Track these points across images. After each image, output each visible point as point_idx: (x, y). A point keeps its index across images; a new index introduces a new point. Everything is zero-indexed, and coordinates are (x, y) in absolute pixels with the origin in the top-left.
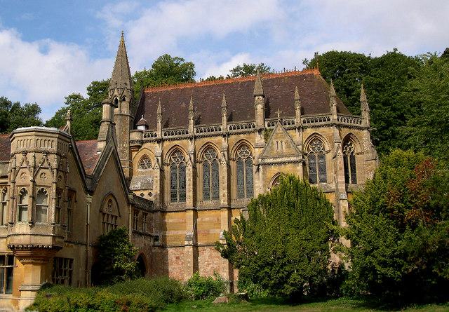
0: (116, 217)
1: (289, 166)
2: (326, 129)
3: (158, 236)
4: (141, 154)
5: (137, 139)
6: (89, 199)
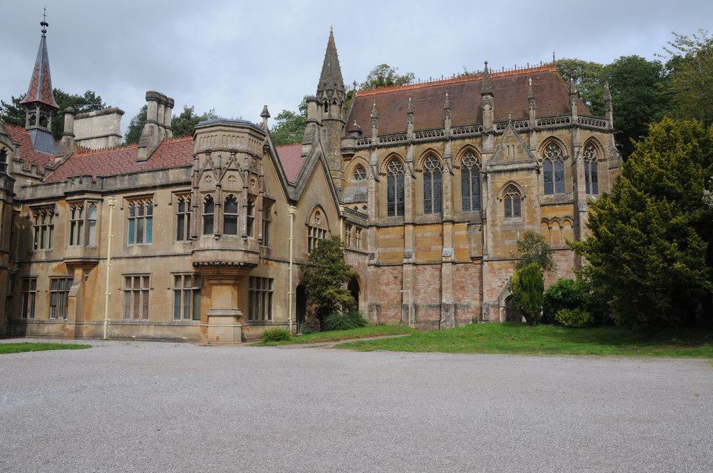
0: (325, 231)
1: (520, 173)
2: (565, 132)
3: (373, 254)
4: (354, 163)
5: (350, 146)
6: (291, 209)
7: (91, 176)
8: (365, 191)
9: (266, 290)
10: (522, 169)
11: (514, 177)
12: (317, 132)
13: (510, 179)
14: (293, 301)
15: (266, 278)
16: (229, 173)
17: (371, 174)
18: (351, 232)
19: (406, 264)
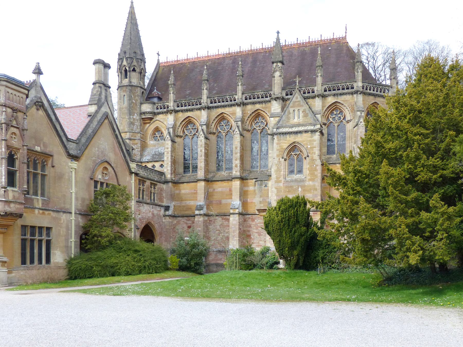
1: (304, 135)
2: (348, 97)
3: (169, 207)
4: (152, 127)
5: (148, 110)
6: (74, 164)
9: (43, 238)
10: (306, 132)
11: (299, 138)
13: (295, 141)
14: (75, 248)
15: (44, 227)
17: (168, 136)
18: (145, 187)
19: (197, 215)
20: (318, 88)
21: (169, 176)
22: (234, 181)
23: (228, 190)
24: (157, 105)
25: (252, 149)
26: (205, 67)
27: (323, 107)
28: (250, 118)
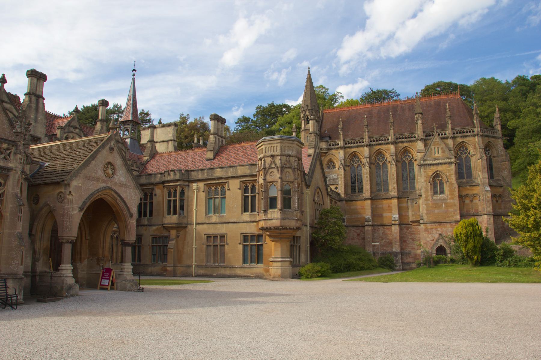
0: (321, 205)
1: (444, 166)
2: (471, 139)
5: (324, 147)
7: (182, 170)
8: (336, 177)
10: (445, 163)
11: (440, 168)
12: (316, 140)
13: (437, 170)
16: (285, 170)
19: (367, 225)
20: (449, 132)
21: (343, 196)
22: (393, 200)
23: (387, 206)
24: (330, 143)
25: (403, 176)
26: (365, 116)
27: (454, 145)
28: (400, 153)
